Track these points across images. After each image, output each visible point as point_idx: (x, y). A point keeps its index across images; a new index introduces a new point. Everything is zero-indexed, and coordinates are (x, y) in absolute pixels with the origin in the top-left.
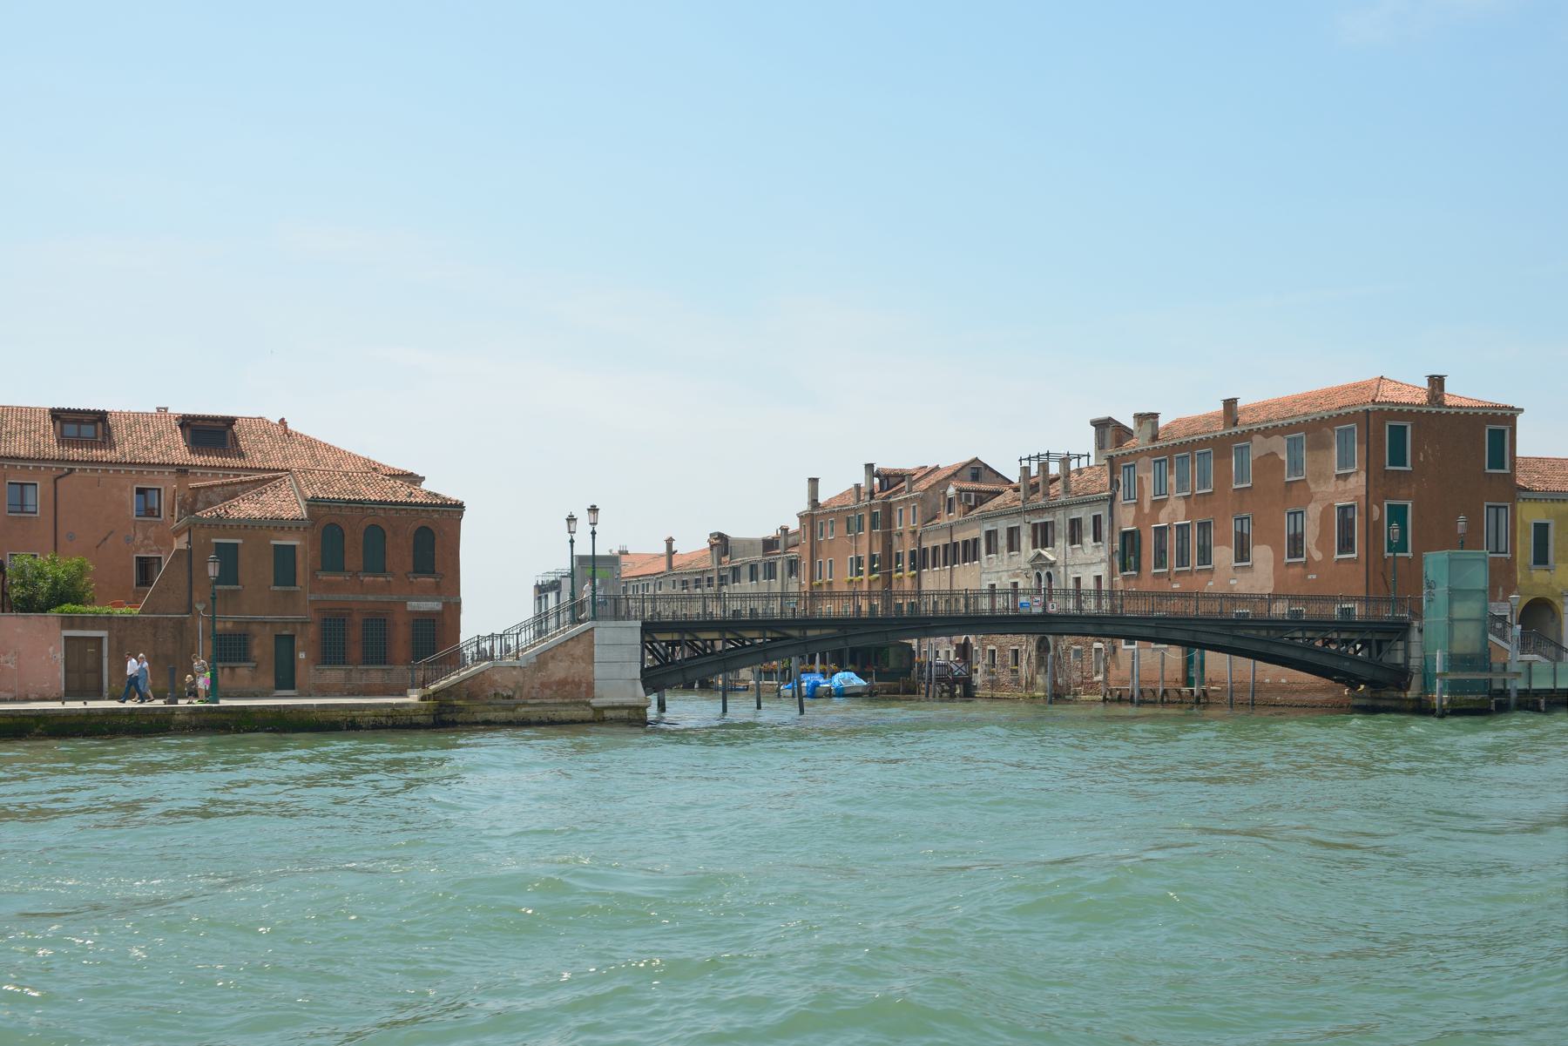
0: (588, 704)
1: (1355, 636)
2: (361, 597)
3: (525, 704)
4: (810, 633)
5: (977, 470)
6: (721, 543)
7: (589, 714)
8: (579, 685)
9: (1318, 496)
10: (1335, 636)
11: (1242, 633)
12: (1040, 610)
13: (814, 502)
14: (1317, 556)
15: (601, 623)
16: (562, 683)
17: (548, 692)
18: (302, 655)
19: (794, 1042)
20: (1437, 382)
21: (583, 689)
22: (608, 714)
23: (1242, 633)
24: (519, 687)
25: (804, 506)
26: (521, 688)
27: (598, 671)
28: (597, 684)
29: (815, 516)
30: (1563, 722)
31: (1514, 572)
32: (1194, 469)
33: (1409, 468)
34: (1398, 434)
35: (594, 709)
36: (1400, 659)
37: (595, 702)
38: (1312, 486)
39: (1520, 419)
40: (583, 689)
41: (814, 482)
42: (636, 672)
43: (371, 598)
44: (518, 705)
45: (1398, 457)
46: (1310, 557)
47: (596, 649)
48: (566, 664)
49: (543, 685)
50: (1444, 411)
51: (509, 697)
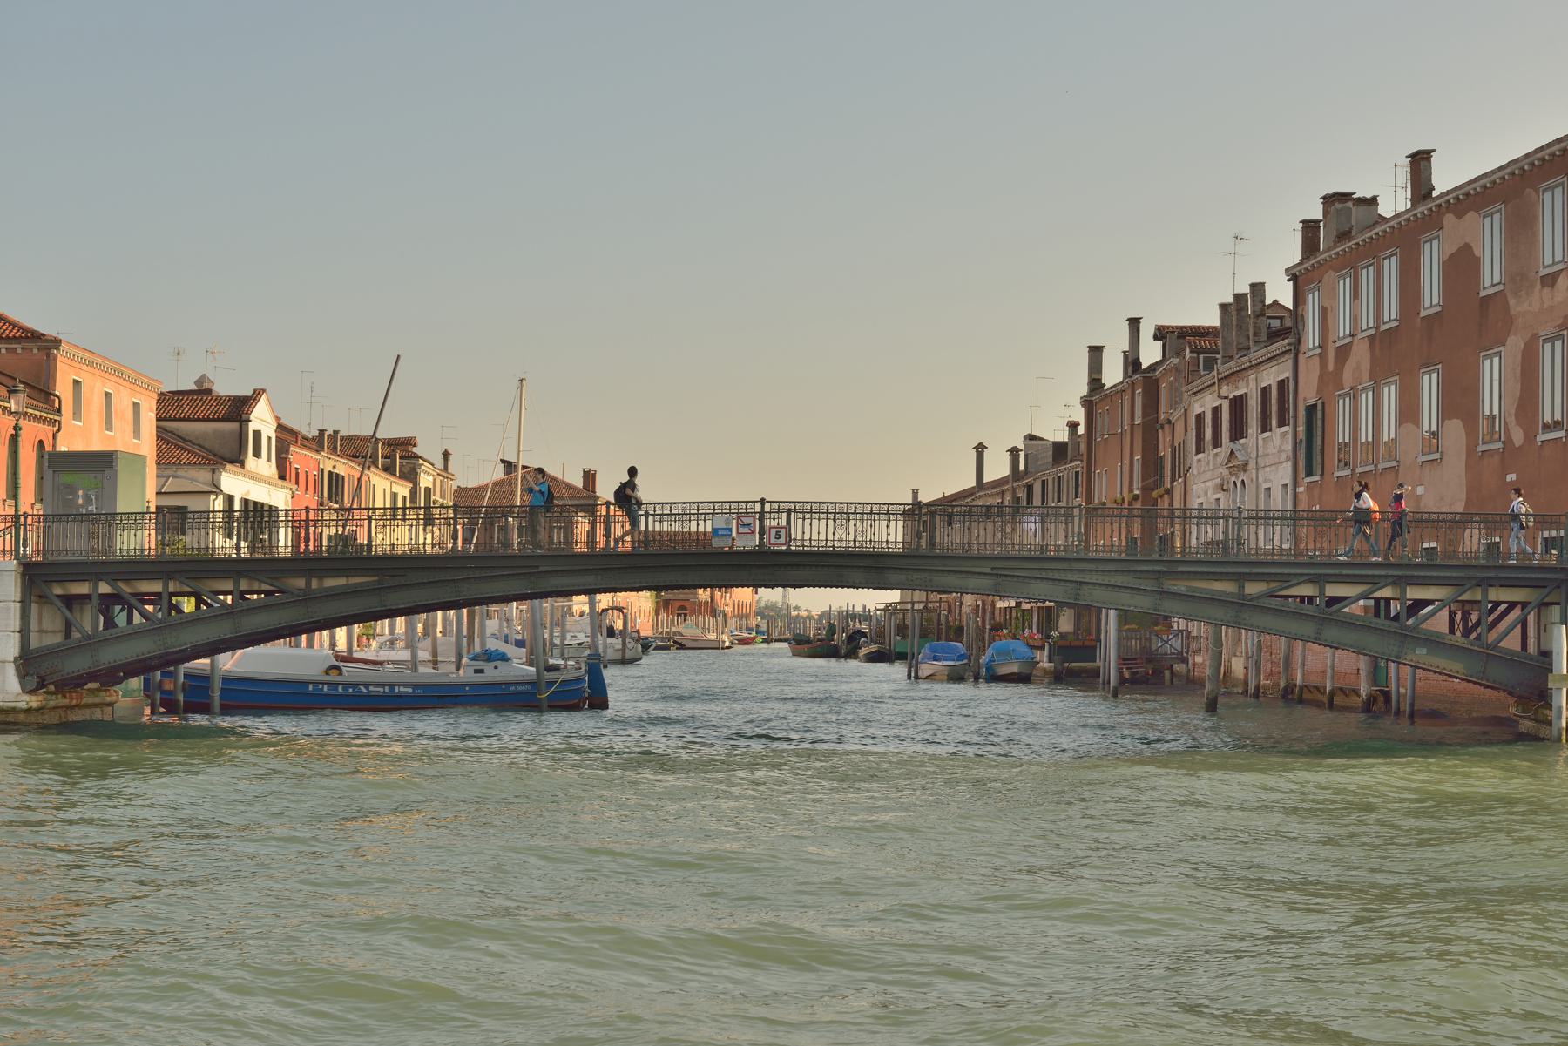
11: (1181, 586)
13: (1095, 383)
23: (1181, 586)
25: (1084, 390)
32: (1367, 276)
38: (1512, 302)
46: (1508, 442)
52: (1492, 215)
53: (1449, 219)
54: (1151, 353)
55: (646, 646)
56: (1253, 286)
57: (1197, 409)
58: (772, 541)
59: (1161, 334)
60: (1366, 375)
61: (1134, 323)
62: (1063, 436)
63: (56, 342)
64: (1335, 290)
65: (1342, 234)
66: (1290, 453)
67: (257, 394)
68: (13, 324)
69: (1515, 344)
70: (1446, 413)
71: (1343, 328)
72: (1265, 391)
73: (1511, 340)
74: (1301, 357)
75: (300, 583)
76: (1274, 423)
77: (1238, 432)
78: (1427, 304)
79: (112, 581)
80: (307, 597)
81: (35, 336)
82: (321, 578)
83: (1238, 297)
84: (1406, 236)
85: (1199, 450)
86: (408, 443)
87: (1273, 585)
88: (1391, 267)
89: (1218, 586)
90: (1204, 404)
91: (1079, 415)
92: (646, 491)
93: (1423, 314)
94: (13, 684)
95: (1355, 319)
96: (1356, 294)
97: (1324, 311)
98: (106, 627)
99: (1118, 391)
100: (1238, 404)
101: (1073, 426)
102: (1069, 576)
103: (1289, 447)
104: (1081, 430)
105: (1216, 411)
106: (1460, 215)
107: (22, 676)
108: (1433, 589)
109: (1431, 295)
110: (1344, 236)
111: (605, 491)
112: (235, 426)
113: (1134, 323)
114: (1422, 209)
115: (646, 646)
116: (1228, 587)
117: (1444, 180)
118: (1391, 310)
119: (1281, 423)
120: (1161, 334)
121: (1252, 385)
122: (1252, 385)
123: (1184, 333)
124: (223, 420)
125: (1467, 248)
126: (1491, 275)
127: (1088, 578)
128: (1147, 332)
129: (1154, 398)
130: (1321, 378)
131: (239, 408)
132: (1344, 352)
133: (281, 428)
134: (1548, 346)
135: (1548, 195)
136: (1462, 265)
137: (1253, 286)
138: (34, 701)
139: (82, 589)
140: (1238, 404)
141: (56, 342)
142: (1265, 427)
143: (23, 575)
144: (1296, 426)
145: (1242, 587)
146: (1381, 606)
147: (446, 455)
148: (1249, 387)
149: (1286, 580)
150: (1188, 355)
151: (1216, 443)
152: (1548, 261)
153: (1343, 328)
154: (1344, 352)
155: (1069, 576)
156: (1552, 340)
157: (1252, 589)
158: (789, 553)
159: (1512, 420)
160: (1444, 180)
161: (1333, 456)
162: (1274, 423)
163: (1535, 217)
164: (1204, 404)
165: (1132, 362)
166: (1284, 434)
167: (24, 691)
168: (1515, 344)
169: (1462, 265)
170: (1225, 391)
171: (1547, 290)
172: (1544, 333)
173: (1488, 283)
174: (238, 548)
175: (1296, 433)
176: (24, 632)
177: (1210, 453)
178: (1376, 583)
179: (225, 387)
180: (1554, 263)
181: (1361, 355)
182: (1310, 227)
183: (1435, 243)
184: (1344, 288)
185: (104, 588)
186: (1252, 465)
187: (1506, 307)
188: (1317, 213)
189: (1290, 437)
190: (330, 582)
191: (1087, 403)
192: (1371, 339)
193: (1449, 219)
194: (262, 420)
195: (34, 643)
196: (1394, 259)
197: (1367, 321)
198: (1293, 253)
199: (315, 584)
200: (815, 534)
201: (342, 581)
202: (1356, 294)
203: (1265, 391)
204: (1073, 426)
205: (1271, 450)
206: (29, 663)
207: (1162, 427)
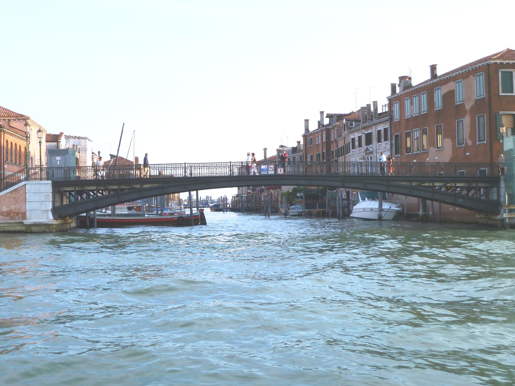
0: (22, 223)
1: (480, 185)
4: (146, 186)
5: (362, 108)
7: (23, 228)
8: (18, 214)
11: (395, 183)
12: (273, 173)
13: (307, 130)
14: (470, 143)
15: (29, 182)
18: (457, 209)
19: (160, 385)
22: (34, 229)
23: (395, 183)
25: (303, 132)
27: (28, 206)
28: (27, 213)
29: (307, 136)
30: (3, 229)
32: (416, 100)
35: (26, 225)
36: (495, 197)
37: (26, 222)
41: (307, 121)
46: (466, 144)
52: (459, 82)
54: (326, 121)
57: (352, 137)
58: (188, 175)
59: (329, 116)
61: (322, 113)
62: (295, 145)
65: (404, 91)
66: (389, 149)
72: (379, 132)
76: (383, 140)
77: (369, 141)
78: (437, 106)
81: (22, 116)
85: (353, 148)
87: (419, 183)
88: (424, 97)
89: (404, 183)
92: (150, 162)
93: (436, 109)
94: (51, 217)
96: (412, 104)
98: (81, 199)
99: (315, 133)
100: (369, 137)
101: (299, 142)
104: (302, 143)
105: (360, 138)
107: (54, 215)
108: (404, 185)
109: (438, 103)
111: (141, 162)
112: (55, 143)
113: (322, 113)
117: (440, 72)
118: (425, 108)
119: (386, 140)
123: (340, 117)
128: (325, 115)
136: (449, 96)
138: (55, 222)
140: (369, 137)
142: (379, 141)
145: (411, 184)
146: (448, 189)
147: (99, 152)
148: (373, 131)
149: (423, 182)
150: (344, 121)
151: (360, 145)
157: (414, 184)
160: (440, 72)
161: (404, 150)
162: (383, 140)
165: (320, 124)
166: (387, 143)
167: (55, 219)
169: (449, 96)
170: (363, 131)
173: (458, 101)
174: (322, 171)
176: (54, 202)
177: (357, 150)
178: (448, 182)
180: (480, 96)
182: (393, 87)
183: (439, 90)
186: (374, 152)
188: (397, 82)
189: (389, 144)
191: (305, 137)
196: (425, 95)
198: (389, 93)
201: (156, 185)
202: (412, 104)
203: (379, 132)
204: (299, 142)
205: (381, 147)
206: (55, 211)
207: (332, 142)
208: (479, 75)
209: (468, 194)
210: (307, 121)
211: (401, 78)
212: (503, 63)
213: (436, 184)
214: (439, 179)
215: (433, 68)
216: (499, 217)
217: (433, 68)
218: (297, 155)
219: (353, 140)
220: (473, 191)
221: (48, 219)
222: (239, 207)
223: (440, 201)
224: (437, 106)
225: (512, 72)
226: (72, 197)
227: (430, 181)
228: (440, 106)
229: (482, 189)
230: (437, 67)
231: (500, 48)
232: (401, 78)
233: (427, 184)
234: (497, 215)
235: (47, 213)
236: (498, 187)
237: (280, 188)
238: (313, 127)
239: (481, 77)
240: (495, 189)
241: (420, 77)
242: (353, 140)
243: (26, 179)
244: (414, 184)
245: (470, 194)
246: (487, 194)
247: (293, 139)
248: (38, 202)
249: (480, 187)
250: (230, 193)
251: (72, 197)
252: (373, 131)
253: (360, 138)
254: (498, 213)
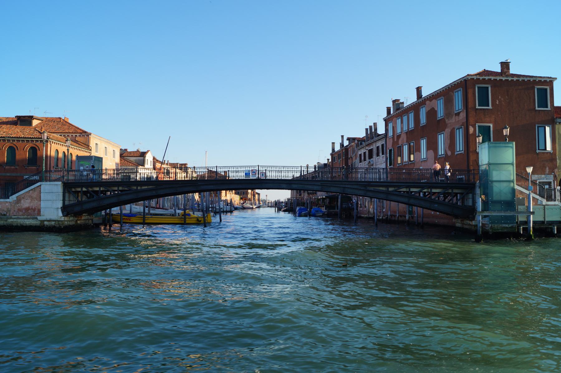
1: (455, 191)
2: (4, 174)
3: (11, 218)
6: (138, 151)
8: (34, 210)
9: (449, 125)
10: (450, 191)
11: (372, 188)
13: (333, 150)
15: (43, 183)
16: (27, 209)
17: (21, 213)
20: (505, 65)
21: (36, 212)
23: (372, 188)
24: (9, 210)
25: (331, 152)
26: (10, 211)
27: (43, 204)
28: (42, 210)
31: (556, 160)
32: (405, 118)
33: (490, 107)
34: (483, 93)
36: (470, 203)
38: (447, 120)
39: (555, 83)
40: (36, 212)
41: (333, 143)
42: (60, 205)
43: (8, 174)
44: (8, 218)
45: (484, 101)
47: (42, 195)
48: (29, 201)
49: (19, 210)
50: (510, 79)
51: (4, 215)
53: (428, 102)
54: (346, 143)
55: (236, 209)
56: (374, 123)
57: (360, 153)
59: (349, 139)
60: (405, 141)
61: (342, 136)
62: (326, 162)
63: (90, 134)
64: (396, 123)
65: (397, 111)
67: (148, 151)
68: (81, 130)
69: (448, 130)
70: (428, 149)
71: (399, 131)
72: (378, 148)
73: (447, 130)
74: (388, 139)
75: (135, 188)
77: (371, 156)
79: (86, 187)
80: (137, 191)
81: (85, 132)
82: (141, 186)
83: (371, 127)
84: (415, 108)
86: (185, 164)
88: (412, 116)
89: (381, 188)
90: (362, 152)
91: (330, 157)
93: (421, 125)
94: (61, 214)
95: (402, 128)
96: (402, 122)
97: (393, 127)
100: (371, 151)
102: (342, 186)
103: (385, 159)
104: (330, 161)
105: (365, 153)
106: (431, 101)
107: (63, 212)
109: (423, 120)
110: (398, 109)
113: (342, 136)
114: (420, 100)
115: (236, 209)
116: (384, 189)
117: (425, 94)
118: (412, 125)
120: (349, 139)
121: (374, 146)
122: (374, 146)
123: (354, 139)
124: (140, 157)
125: (433, 109)
126: (440, 114)
127: (347, 186)
128: (345, 139)
129: (344, 155)
130: (393, 143)
131: (143, 154)
132: (399, 137)
133: (154, 158)
134: (458, 131)
135: (457, 93)
136: (432, 113)
137: (374, 123)
138: (63, 219)
139: (79, 189)
140: (371, 151)
141: (90, 134)
143: (63, 186)
144: (386, 154)
145: (388, 189)
148: (374, 147)
149: (399, 187)
151: (365, 160)
152: (457, 109)
153: (399, 131)
154: (399, 137)
155: (342, 186)
156: (459, 129)
157: (391, 189)
158: (266, 180)
159: (447, 149)
160: (425, 94)
163: (453, 99)
164: (362, 152)
165: (342, 145)
167: (63, 216)
168: (448, 130)
169: (432, 113)
170: (367, 148)
171: (457, 117)
172: (456, 127)
173: (439, 116)
175: (386, 156)
176: (64, 200)
178: (423, 188)
179: (142, 150)
181: (404, 137)
182: (389, 109)
184: (399, 121)
185: (84, 189)
186: (374, 164)
187: (445, 122)
189: (385, 157)
190: (143, 188)
191: (332, 155)
192: (406, 133)
193: (428, 102)
194: (149, 158)
195: (67, 203)
197: (405, 128)
198: (385, 115)
199: (139, 188)
200: (271, 175)
201: (146, 187)
203: (378, 148)
204: (328, 160)
206: (65, 210)
208: (458, 91)
209: (444, 200)
210: (333, 143)
211: (394, 102)
212: (479, 79)
213: (412, 190)
214: (422, 186)
215: (419, 90)
216: (474, 223)
217: (419, 90)
218: (327, 169)
219: (360, 155)
220: (449, 198)
221: (58, 216)
222: (288, 207)
223: (423, 208)
224: (458, 150)
225: (488, 88)
226: (455, 198)
227: (406, 187)
228: (461, 149)
229: (458, 195)
230: (422, 89)
231: (480, 70)
232: (394, 102)
233: (404, 190)
234: (472, 221)
235: (58, 210)
236: (474, 194)
237: (316, 194)
238: (337, 148)
239: (459, 92)
240: (470, 196)
241: (409, 99)
242: (360, 155)
243: (41, 180)
244: (391, 189)
245: (447, 200)
246: (463, 199)
247: (325, 158)
248: (50, 202)
249: (457, 194)
250: (284, 195)
251: (455, 198)
252: (374, 147)
253: (365, 153)
254: (473, 219)
